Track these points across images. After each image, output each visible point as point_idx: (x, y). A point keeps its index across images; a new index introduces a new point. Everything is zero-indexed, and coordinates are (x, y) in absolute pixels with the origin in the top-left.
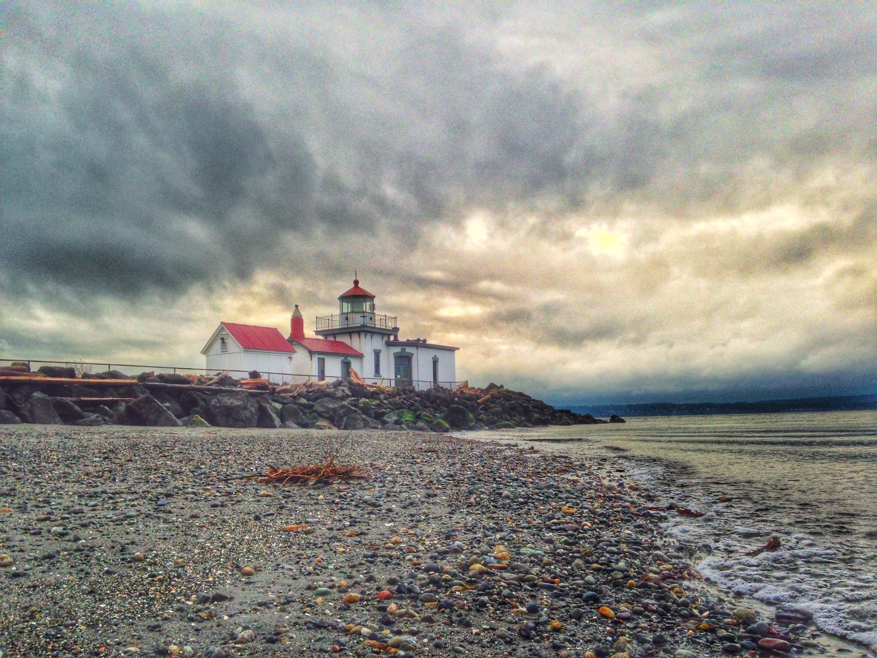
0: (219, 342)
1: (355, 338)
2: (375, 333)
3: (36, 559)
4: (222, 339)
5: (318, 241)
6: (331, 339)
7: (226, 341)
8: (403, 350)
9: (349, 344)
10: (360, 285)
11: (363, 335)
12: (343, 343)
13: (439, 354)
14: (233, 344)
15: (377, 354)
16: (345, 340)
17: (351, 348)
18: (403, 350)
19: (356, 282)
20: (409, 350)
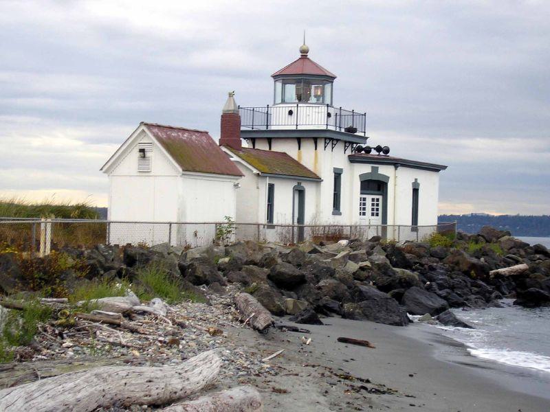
0: (135, 154)
1: (308, 148)
2: (338, 140)
3: (165, 342)
4: (142, 151)
5: (471, 253)
6: (262, 146)
7: (148, 154)
8: (375, 170)
9: (296, 158)
10: (310, 55)
11: (321, 145)
12: (284, 154)
13: (424, 178)
14: (161, 160)
15: (338, 175)
16: (290, 149)
17: (298, 164)
18: (375, 170)
19: (416, 180)
20: (385, 170)
